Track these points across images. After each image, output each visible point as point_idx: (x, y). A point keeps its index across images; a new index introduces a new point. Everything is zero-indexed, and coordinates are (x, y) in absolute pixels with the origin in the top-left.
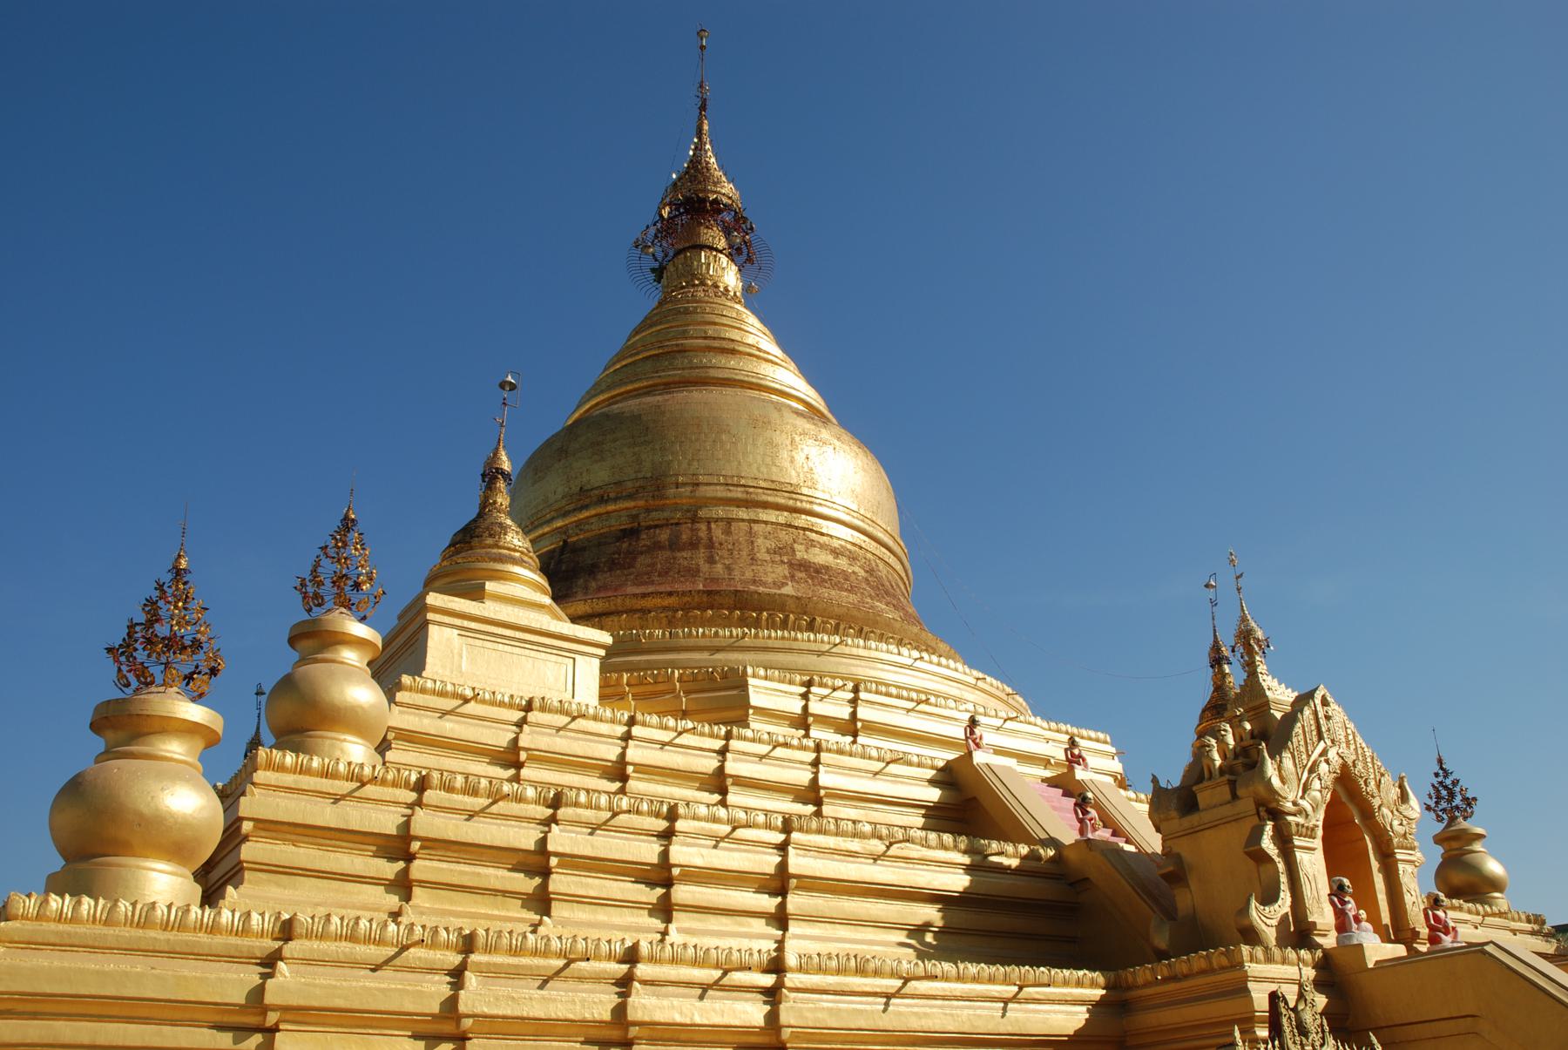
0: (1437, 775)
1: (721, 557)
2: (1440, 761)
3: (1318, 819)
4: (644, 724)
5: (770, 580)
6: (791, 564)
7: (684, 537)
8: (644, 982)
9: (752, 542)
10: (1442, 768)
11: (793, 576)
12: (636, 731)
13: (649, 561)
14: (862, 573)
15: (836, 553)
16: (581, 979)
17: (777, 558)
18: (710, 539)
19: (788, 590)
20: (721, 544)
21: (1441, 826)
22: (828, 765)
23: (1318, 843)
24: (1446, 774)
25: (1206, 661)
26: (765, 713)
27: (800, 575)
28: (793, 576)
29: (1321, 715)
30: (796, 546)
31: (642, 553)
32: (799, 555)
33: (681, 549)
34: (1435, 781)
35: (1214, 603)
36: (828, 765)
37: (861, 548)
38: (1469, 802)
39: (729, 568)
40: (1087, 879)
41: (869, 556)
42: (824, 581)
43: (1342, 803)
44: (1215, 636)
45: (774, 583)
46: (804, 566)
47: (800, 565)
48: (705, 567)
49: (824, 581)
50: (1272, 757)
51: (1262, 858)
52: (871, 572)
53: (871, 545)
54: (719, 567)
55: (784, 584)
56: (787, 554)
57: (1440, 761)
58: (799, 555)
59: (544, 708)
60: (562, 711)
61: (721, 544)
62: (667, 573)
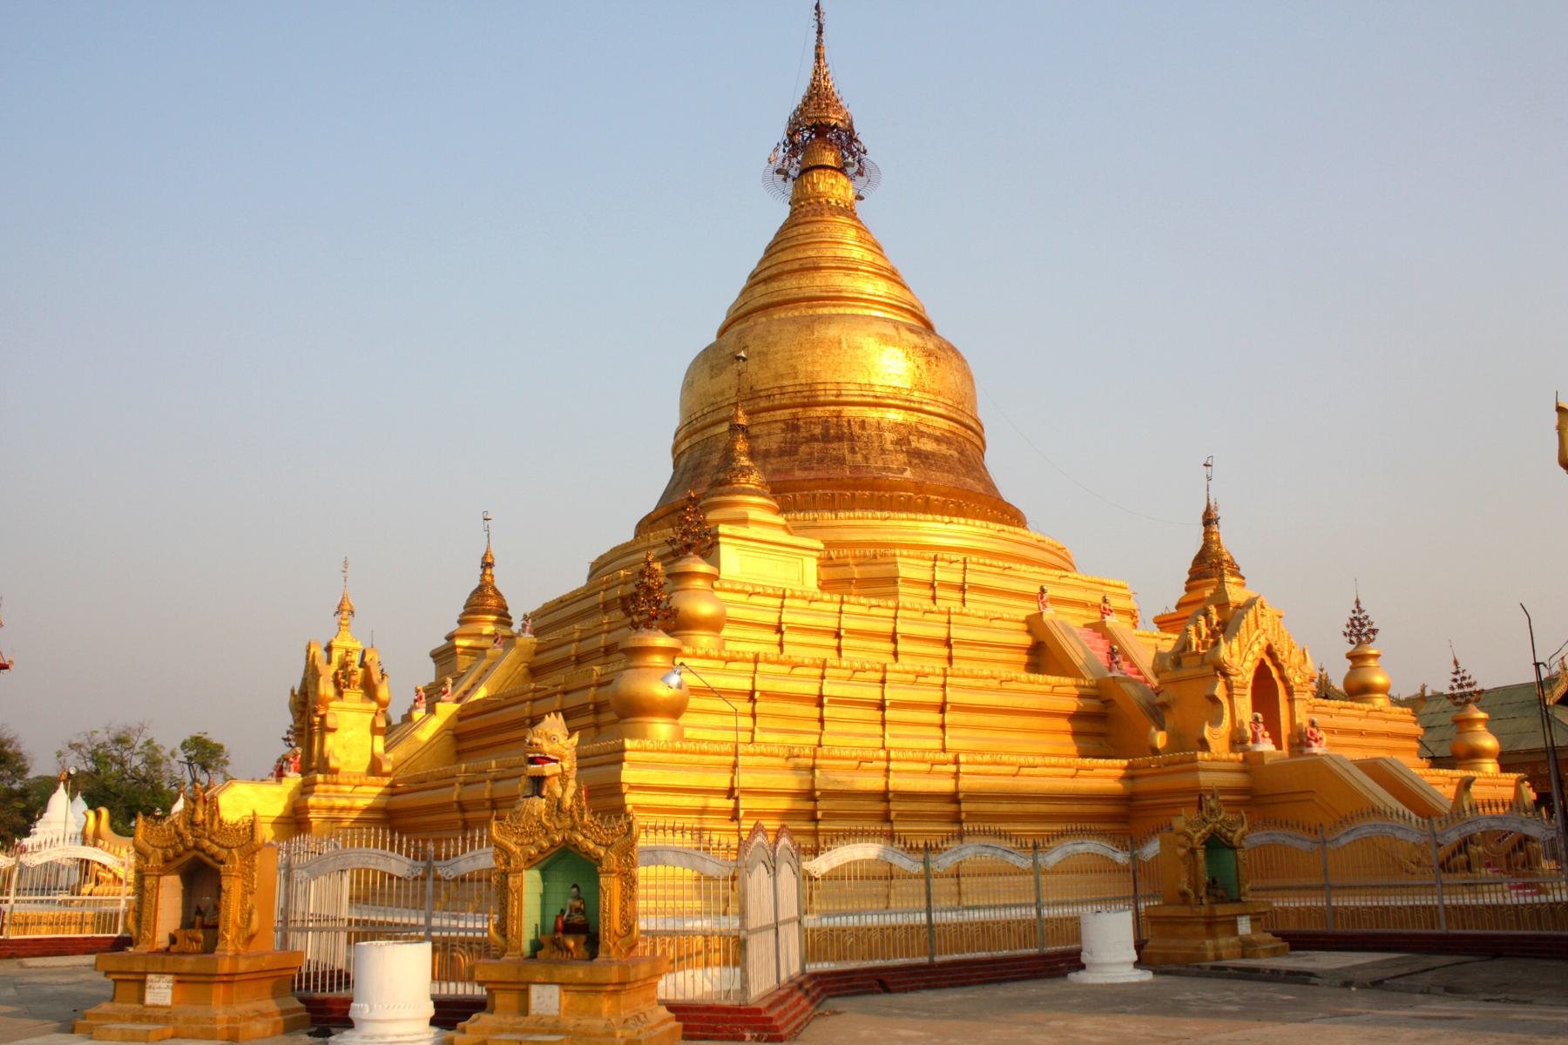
0: (1354, 612)
1: (860, 449)
2: (1358, 602)
3: (1249, 677)
4: (849, 603)
5: (895, 467)
6: (908, 452)
7: (832, 431)
8: (895, 772)
9: (881, 436)
10: (1358, 607)
11: (910, 463)
12: (845, 607)
13: (808, 450)
14: (956, 455)
15: (938, 440)
16: (866, 770)
17: (898, 448)
18: (851, 433)
19: (908, 474)
20: (859, 437)
21: (1353, 646)
22: (955, 624)
23: (1249, 691)
24: (1361, 611)
25: (1200, 521)
26: (910, 582)
27: (916, 461)
28: (910, 463)
29: (1259, 614)
30: (911, 437)
31: (802, 443)
32: (914, 444)
33: (830, 442)
34: (1352, 615)
35: (1209, 479)
36: (955, 624)
37: (954, 433)
38: (1374, 631)
39: (866, 458)
40: (1112, 700)
41: (960, 439)
42: (931, 465)
43: (1267, 668)
44: (1208, 499)
45: (898, 469)
46: (917, 453)
47: (915, 453)
48: (848, 456)
49: (931, 465)
50: (1226, 641)
51: (1214, 700)
52: (961, 453)
53: (961, 430)
54: (859, 457)
55: (905, 470)
56: (905, 444)
57: (1358, 602)
58: (914, 444)
59: (793, 596)
60: (804, 598)
61: (859, 437)
62: (822, 461)
